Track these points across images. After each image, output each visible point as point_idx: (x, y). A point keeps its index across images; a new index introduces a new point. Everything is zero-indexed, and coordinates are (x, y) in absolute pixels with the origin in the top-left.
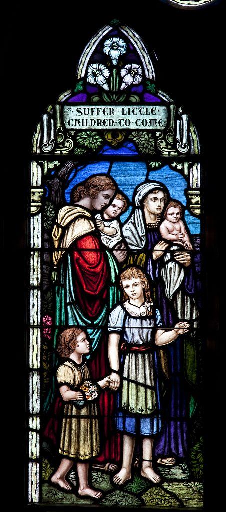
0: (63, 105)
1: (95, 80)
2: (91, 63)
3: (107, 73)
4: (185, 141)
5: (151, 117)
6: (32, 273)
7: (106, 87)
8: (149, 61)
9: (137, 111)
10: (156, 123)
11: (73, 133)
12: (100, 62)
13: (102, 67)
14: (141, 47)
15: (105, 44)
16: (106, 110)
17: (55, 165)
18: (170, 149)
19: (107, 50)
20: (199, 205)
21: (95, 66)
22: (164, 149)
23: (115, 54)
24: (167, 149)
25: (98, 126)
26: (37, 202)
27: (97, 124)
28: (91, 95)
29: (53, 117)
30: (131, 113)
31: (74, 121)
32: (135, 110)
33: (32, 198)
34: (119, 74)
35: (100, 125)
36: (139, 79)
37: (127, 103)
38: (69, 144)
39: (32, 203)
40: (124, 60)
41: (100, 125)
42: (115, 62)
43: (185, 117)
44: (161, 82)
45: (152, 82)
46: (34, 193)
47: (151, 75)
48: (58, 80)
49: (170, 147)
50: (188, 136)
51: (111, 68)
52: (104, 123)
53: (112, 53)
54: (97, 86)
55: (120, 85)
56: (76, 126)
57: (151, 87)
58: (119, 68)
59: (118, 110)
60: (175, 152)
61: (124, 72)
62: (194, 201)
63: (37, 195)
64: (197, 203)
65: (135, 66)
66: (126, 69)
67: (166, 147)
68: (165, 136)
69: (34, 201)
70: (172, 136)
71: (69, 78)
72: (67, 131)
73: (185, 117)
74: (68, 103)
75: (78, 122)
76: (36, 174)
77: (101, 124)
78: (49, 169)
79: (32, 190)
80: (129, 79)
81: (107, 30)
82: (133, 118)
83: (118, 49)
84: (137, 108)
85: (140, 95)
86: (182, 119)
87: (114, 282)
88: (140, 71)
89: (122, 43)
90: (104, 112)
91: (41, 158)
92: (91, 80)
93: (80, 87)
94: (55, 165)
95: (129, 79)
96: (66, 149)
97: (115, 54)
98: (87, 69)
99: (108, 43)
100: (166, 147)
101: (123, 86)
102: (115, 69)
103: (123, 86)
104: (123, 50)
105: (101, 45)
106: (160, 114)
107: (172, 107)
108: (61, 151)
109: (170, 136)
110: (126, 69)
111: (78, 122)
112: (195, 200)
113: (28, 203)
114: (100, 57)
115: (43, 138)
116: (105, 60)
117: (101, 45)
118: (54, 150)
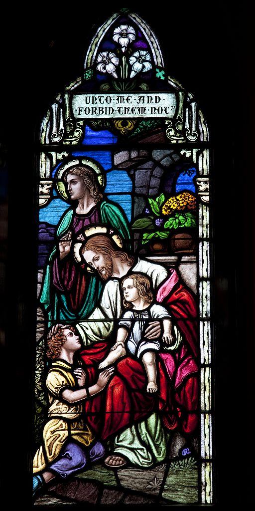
0: (72, 94)
1: (105, 68)
3: (115, 60)
5: (126, 105)
6: (209, 295)
7: (115, 75)
9: (103, 100)
10: (128, 110)
11: (81, 123)
12: (109, 50)
13: (111, 55)
14: (97, 39)
15: (115, 31)
16: (129, 98)
17: (63, 156)
18: (178, 137)
19: (116, 38)
20: (207, 192)
21: (105, 54)
22: (172, 137)
23: (124, 41)
24: (175, 136)
25: (92, 114)
26: (46, 194)
27: (91, 112)
28: (98, 84)
29: (62, 105)
31: (124, 109)
33: (41, 189)
34: (128, 61)
35: (94, 113)
36: (148, 66)
37: (137, 91)
38: (78, 133)
40: (132, 47)
41: (94, 113)
42: (123, 50)
43: (193, 104)
46: (42, 186)
47: (159, 61)
48: (69, 70)
49: (178, 135)
51: (119, 56)
52: (132, 110)
53: (126, 42)
54: (108, 75)
55: (129, 74)
57: (160, 74)
58: (128, 55)
59: (134, 97)
60: (182, 140)
61: (132, 60)
62: (201, 188)
63: (46, 187)
64: (206, 190)
65: (143, 53)
66: (134, 57)
67: (174, 135)
68: (174, 124)
69: (42, 193)
73: (193, 104)
74: (79, 91)
75: (127, 110)
77: (95, 112)
78: (57, 160)
79: (41, 182)
83: (127, 37)
85: (148, 83)
86: (191, 107)
88: (148, 58)
90: (100, 100)
92: (100, 67)
93: (88, 75)
94: (63, 156)
95: (138, 66)
96: (76, 138)
97: (124, 41)
99: (117, 30)
100: (174, 135)
101: (133, 74)
102: (124, 54)
103: (133, 74)
104: (131, 36)
105: (110, 34)
106: (167, 101)
108: (71, 141)
109: (179, 124)
110: (134, 57)
111: (127, 110)
112: (203, 187)
114: (109, 45)
115: (49, 130)
116: (115, 48)
117: (110, 34)
118: (63, 140)
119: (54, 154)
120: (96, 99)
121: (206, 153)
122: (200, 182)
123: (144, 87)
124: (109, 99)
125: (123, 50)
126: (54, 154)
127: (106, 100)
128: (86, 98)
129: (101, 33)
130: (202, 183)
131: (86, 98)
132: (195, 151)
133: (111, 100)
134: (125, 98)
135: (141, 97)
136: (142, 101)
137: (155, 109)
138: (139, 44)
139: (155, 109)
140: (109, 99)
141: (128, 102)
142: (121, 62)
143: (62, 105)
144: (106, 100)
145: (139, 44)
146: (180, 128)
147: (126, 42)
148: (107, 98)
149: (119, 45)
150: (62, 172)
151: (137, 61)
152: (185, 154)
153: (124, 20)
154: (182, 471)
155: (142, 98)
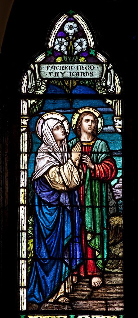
2: (57, 37)
3: (66, 44)
4: (112, 86)
8: (91, 36)
13: (63, 40)
19: (66, 29)
21: (60, 40)
23: (71, 32)
30: (56, 69)
32: (87, 67)
33: (22, 122)
34: (73, 45)
39: (22, 125)
42: (71, 37)
43: (112, 71)
44: (98, 48)
45: (93, 49)
47: (92, 44)
50: (115, 84)
53: (71, 29)
56: (56, 76)
70: (104, 82)
71: (44, 48)
72: (42, 79)
73: (112, 71)
74: (44, 62)
76: (24, 107)
80: (79, 48)
81: (62, 20)
82: (75, 70)
84: (59, 66)
87: (105, 231)
89: (75, 26)
90: (86, 68)
91: (29, 96)
92: (57, 47)
95: (79, 48)
97: (71, 32)
98: (55, 41)
102: (71, 42)
107: (104, 65)
113: (19, 126)
114: (62, 33)
119: (29, 101)
120: (63, 68)
121: (119, 102)
122: (117, 120)
123: (82, 59)
124: (92, 67)
125: (71, 37)
126: (29, 101)
127: (91, 68)
128: (77, 66)
129: (57, 27)
130: (118, 120)
131: (77, 66)
132: (114, 101)
133: (93, 68)
134: (90, 66)
135: (53, 66)
136: (53, 69)
137: (84, 73)
138: (80, 34)
139: (84, 73)
140: (92, 67)
141: (66, 69)
142: (69, 44)
143: (34, 72)
144: (91, 68)
145: (80, 34)
146: (104, 84)
147: (71, 29)
148: (91, 67)
149: (68, 35)
150: (86, 110)
151: (63, 45)
152: (109, 102)
153: (71, 19)
154: (96, 305)
155: (53, 67)
